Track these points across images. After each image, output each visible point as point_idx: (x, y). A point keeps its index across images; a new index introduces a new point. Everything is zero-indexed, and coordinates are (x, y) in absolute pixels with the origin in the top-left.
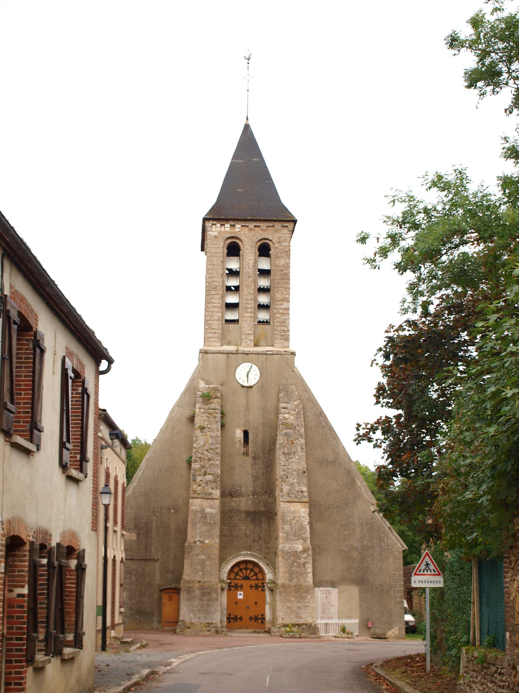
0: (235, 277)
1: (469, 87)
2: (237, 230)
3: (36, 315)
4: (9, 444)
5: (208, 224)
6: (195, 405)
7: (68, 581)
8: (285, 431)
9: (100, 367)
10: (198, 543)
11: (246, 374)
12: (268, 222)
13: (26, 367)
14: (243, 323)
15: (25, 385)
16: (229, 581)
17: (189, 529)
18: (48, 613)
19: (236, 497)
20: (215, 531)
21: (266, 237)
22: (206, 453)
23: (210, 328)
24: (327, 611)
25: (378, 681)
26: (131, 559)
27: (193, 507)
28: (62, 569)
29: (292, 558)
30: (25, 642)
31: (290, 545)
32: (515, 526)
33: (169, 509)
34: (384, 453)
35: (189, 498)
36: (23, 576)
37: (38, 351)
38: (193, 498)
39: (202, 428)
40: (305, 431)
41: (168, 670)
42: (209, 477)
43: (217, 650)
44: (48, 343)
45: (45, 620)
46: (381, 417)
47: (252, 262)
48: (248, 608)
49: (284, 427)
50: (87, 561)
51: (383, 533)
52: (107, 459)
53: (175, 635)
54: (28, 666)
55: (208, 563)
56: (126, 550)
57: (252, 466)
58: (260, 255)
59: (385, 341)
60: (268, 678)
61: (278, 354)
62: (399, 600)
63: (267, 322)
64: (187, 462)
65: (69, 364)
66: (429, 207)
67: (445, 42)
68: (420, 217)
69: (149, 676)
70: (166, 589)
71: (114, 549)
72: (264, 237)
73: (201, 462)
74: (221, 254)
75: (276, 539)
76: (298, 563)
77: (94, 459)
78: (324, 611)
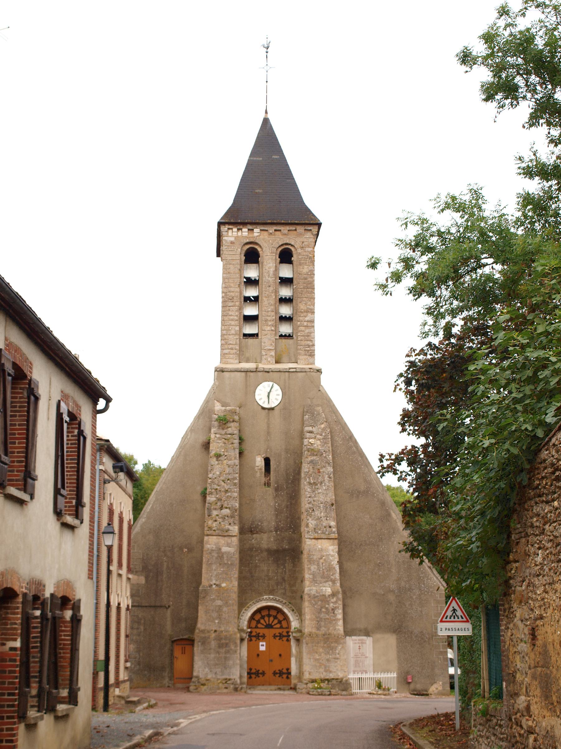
0: (254, 287)
1: (486, 100)
2: (256, 234)
3: (31, 363)
4: (2, 495)
5: (224, 229)
6: (210, 430)
7: (63, 634)
8: (310, 458)
10: (214, 586)
11: (267, 394)
12: (290, 226)
13: (20, 416)
14: (263, 337)
15: (19, 434)
16: (249, 630)
17: (204, 571)
18: (41, 666)
19: (257, 533)
20: (233, 572)
21: (288, 242)
22: (223, 483)
23: (226, 343)
24: (361, 664)
25: (402, 741)
26: (138, 606)
27: (209, 546)
28: (56, 621)
29: (320, 603)
30: (17, 697)
31: (318, 588)
32: (507, 573)
33: (181, 549)
34: (409, 487)
35: (204, 535)
36: (15, 629)
37: (32, 398)
38: (208, 535)
39: (218, 456)
40: (333, 458)
41: (174, 731)
42: (226, 512)
43: (233, 710)
44: (43, 391)
45: (38, 674)
46: (406, 447)
47: (272, 270)
48: (272, 661)
49: (310, 453)
50: (82, 612)
51: (422, 573)
52: (110, 494)
53: (189, 693)
54: (20, 722)
55: (225, 609)
56: (132, 596)
57: (275, 498)
58: (281, 262)
59: (406, 366)
60: (282, 738)
61: (302, 371)
62: (442, 650)
63: (289, 336)
64: (201, 494)
65: (64, 408)
66: (443, 230)
67: (457, 58)
68: (434, 240)
69: (153, 737)
70: (178, 640)
71: (118, 595)
72: (285, 242)
73: (217, 494)
74: (238, 261)
75: (302, 581)
76: (327, 609)
77: (91, 503)
78: (357, 664)
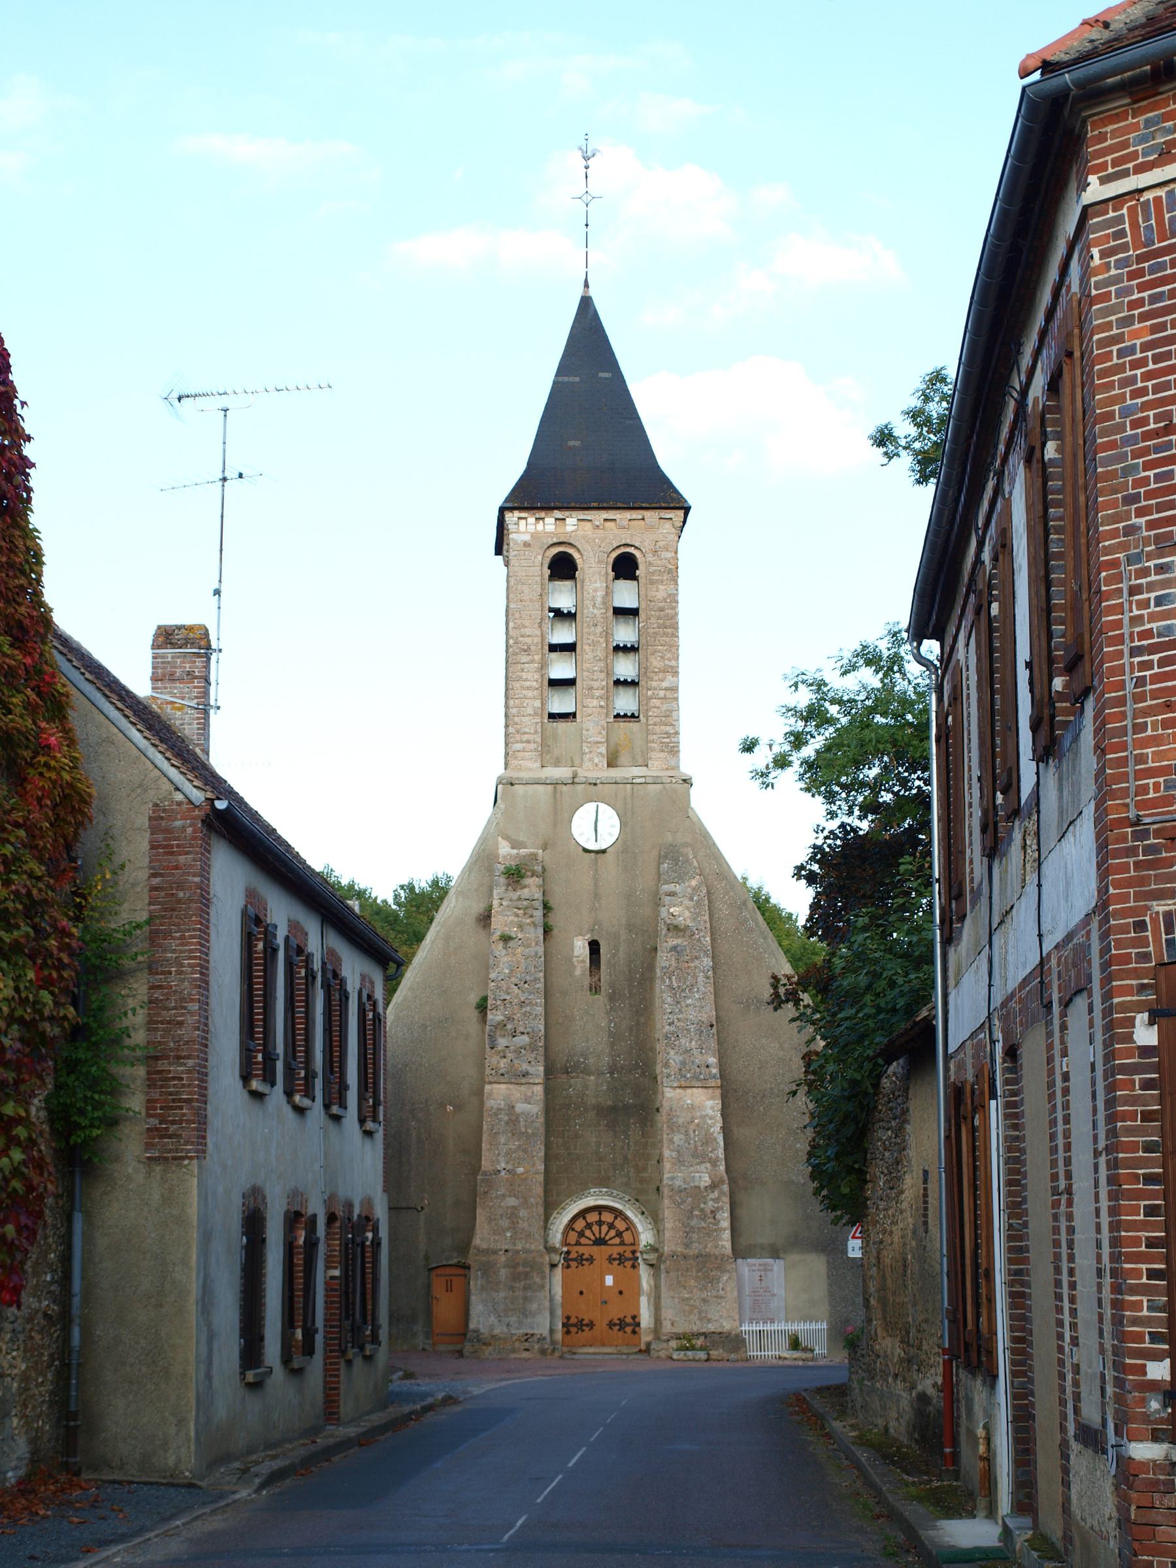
5: (511, 518)
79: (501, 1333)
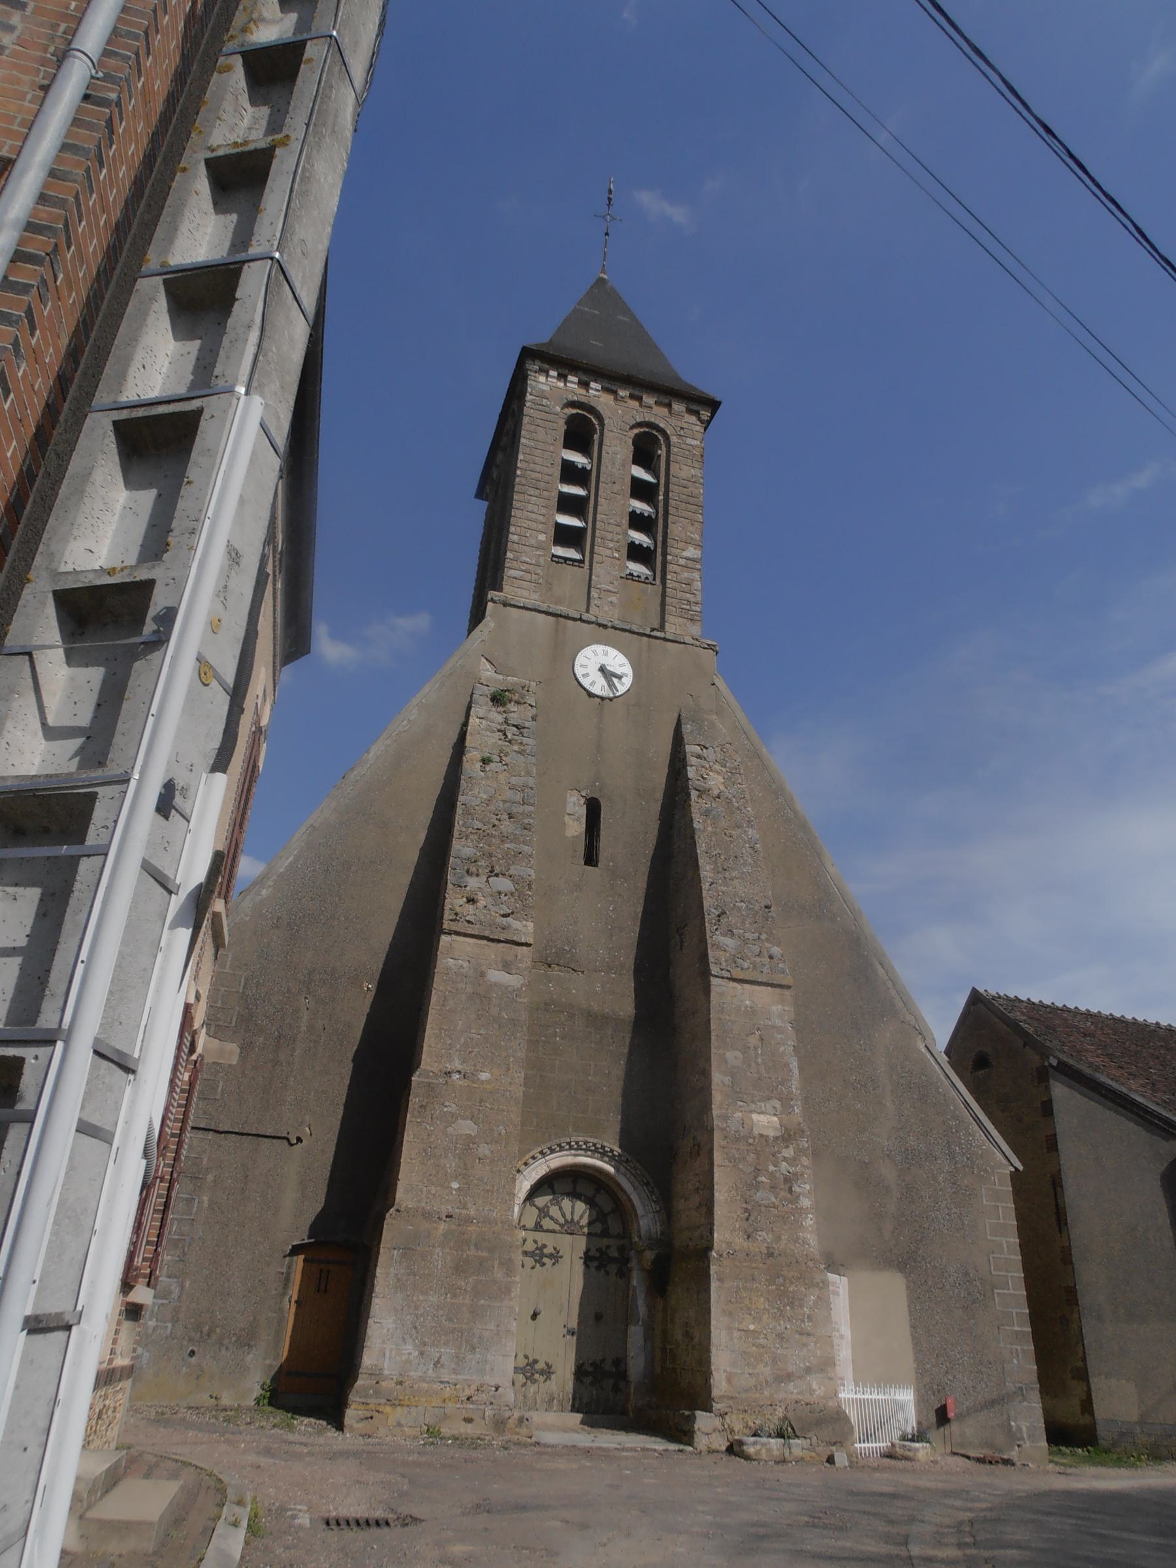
5: (532, 366)
9: (216, 369)
62: (1017, 1328)
79: (422, 1379)
